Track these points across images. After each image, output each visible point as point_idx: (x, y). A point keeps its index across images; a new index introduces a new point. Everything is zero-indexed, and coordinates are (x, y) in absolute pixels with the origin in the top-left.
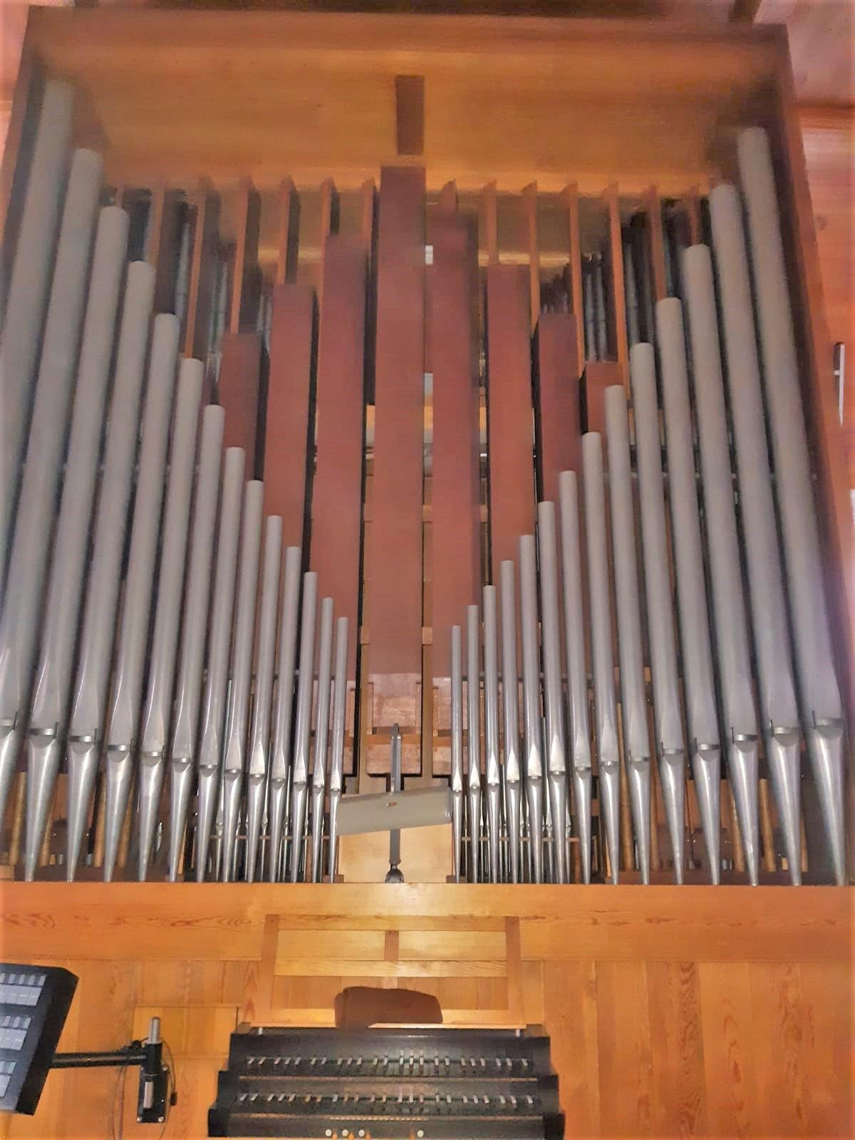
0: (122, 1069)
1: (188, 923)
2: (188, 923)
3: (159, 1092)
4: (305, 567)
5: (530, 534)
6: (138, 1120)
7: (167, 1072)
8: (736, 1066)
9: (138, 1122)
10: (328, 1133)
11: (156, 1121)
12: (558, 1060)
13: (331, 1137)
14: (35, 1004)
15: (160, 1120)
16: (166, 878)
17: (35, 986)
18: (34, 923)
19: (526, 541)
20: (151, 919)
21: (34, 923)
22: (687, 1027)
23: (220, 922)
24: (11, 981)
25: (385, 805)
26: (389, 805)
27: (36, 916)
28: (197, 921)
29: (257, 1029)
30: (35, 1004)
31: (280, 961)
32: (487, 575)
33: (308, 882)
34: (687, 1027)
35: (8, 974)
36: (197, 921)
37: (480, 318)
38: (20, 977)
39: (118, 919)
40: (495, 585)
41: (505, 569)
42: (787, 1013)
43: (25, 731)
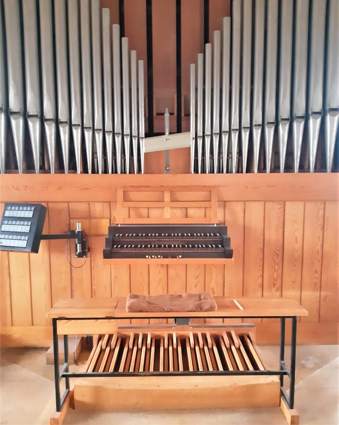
0: (68, 240)
1: (87, 189)
2: (87, 189)
3: (83, 248)
4: (122, 35)
5: (227, 16)
6: (76, 256)
7: (85, 241)
8: (296, 238)
9: (76, 257)
10: (147, 257)
11: (83, 257)
12: (230, 234)
13: (148, 258)
14: (31, 217)
15: (84, 256)
16: (76, 172)
17: (30, 210)
18: (26, 190)
19: (226, 20)
20: (72, 188)
21: (26, 190)
22: (279, 224)
23: (100, 188)
24: (13, 209)
25: (164, 140)
26: (166, 140)
27: (26, 187)
28: (90, 188)
29: (118, 224)
30: (31, 217)
31: (74, 127)
32: (207, 39)
33: (133, 174)
34: (279, 224)
35: (19, 207)
36: (90, 188)
37: (155, 96)
38: (32, 208)
39: (59, 188)
40: (211, 43)
41: (216, 35)
42: (318, 220)
43: (9, 114)
